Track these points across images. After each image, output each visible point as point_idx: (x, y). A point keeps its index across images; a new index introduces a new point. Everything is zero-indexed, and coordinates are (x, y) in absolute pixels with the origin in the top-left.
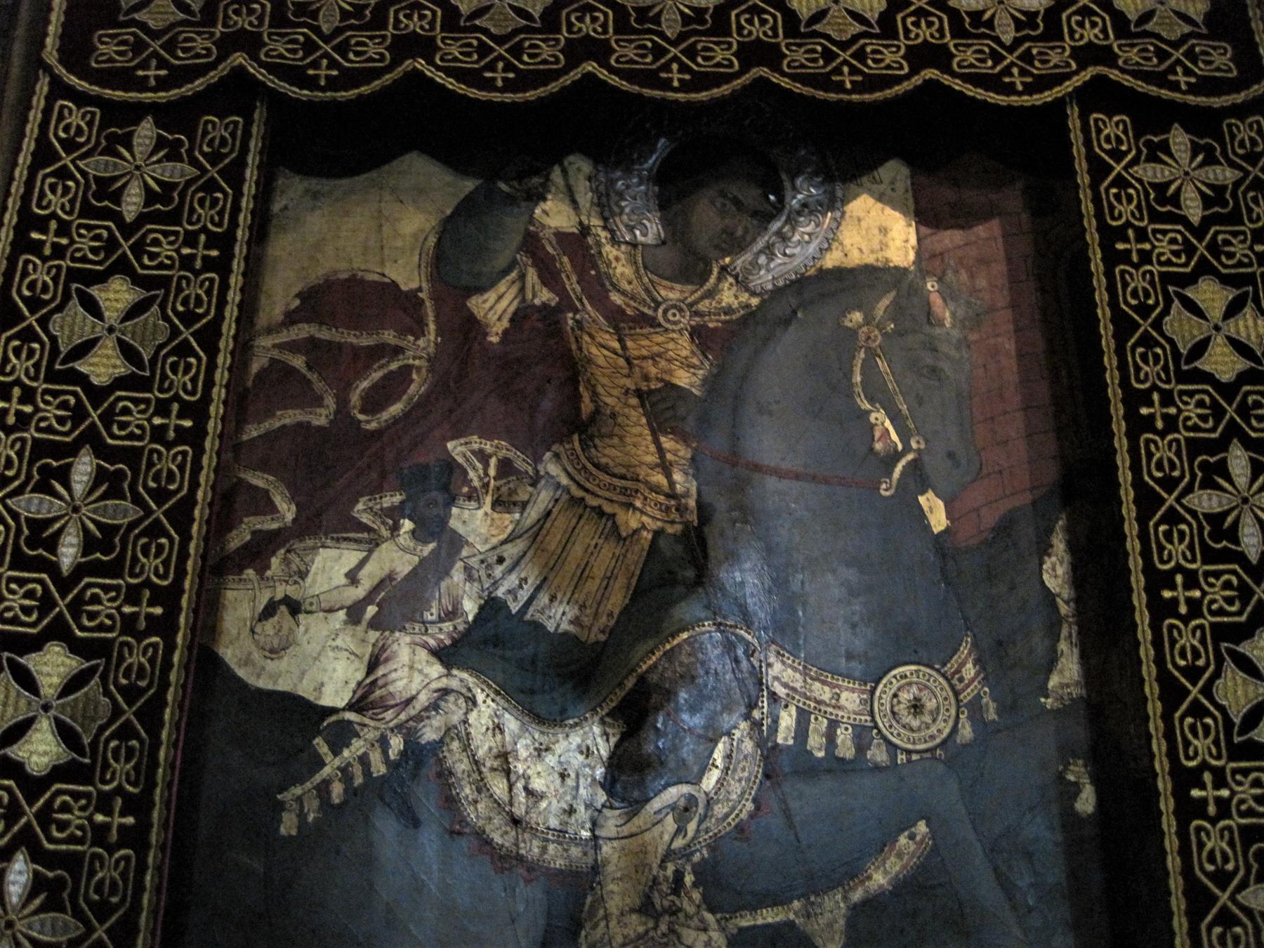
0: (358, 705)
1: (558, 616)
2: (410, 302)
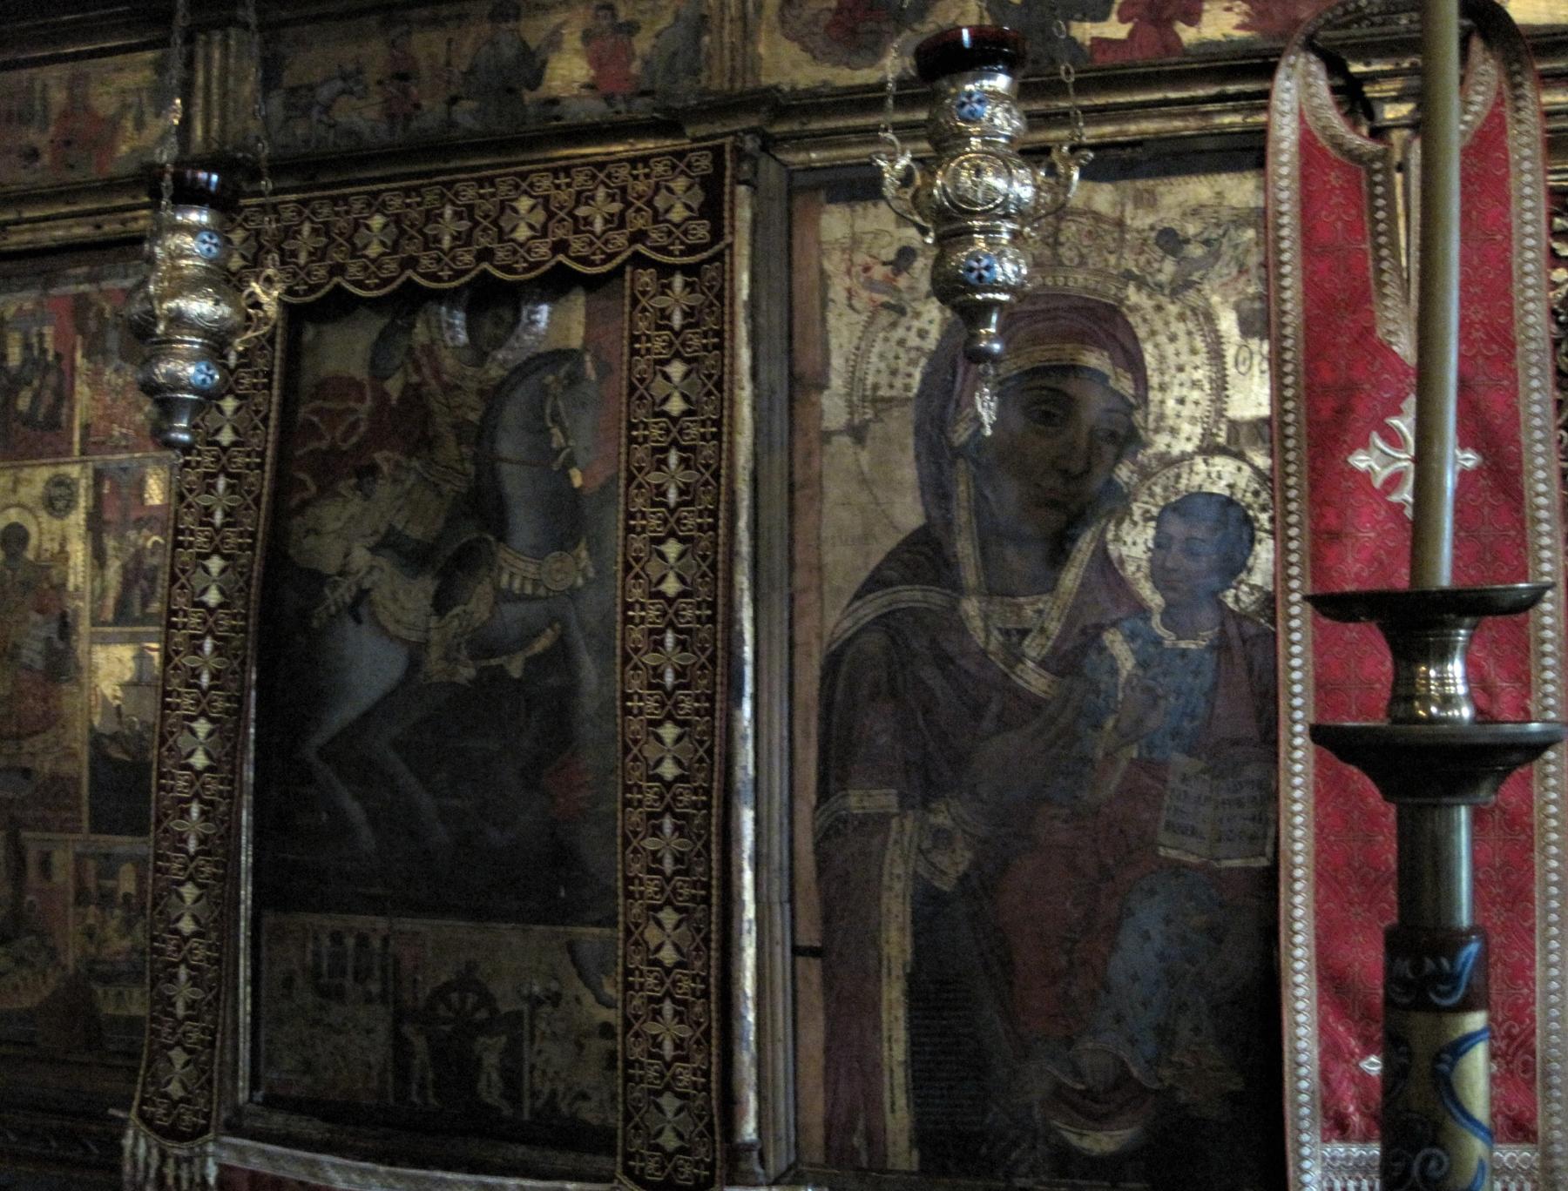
0: (341, 574)
1: (416, 532)
2: (359, 386)
